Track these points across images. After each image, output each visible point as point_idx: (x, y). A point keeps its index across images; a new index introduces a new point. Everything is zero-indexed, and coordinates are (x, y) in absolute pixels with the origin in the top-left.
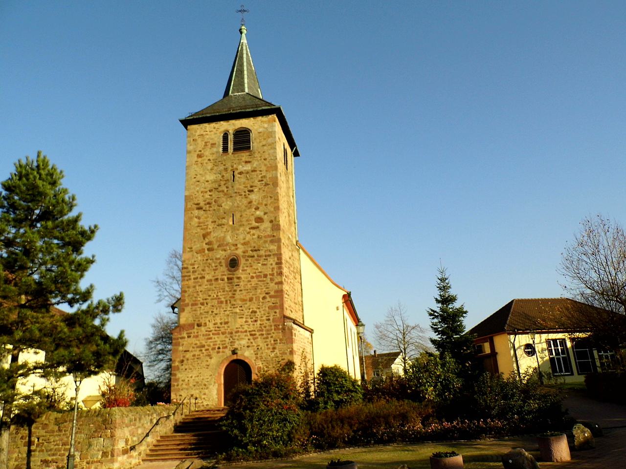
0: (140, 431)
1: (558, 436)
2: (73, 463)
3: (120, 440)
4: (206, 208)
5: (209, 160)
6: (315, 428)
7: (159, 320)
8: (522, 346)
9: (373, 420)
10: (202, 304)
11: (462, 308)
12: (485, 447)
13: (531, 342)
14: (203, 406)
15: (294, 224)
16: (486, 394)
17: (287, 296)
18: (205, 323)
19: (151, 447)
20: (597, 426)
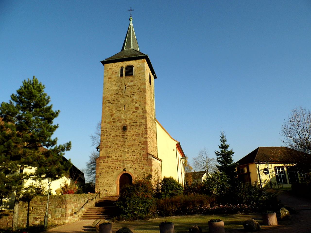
0: (79, 205)
1: (271, 213)
2: (47, 219)
3: (69, 209)
4: (112, 103)
5: (114, 80)
6: (160, 206)
7: (93, 154)
8: (262, 169)
9: (187, 203)
10: (110, 147)
11: (232, 151)
12: (238, 217)
13: (267, 168)
14: (110, 194)
15: (154, 110)
16: (241, 192)
17: (149, 144)
18: (111, 156)
19: (84, 213)
20: (293, 209)
